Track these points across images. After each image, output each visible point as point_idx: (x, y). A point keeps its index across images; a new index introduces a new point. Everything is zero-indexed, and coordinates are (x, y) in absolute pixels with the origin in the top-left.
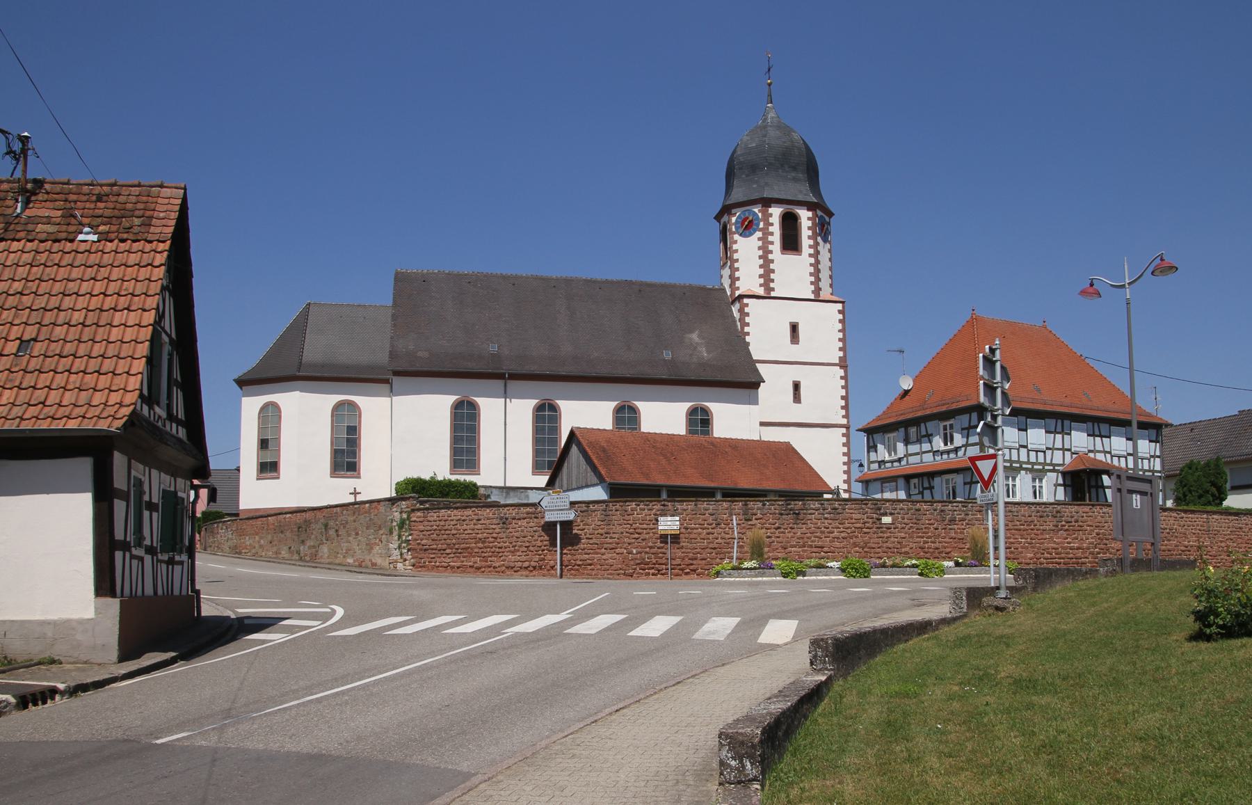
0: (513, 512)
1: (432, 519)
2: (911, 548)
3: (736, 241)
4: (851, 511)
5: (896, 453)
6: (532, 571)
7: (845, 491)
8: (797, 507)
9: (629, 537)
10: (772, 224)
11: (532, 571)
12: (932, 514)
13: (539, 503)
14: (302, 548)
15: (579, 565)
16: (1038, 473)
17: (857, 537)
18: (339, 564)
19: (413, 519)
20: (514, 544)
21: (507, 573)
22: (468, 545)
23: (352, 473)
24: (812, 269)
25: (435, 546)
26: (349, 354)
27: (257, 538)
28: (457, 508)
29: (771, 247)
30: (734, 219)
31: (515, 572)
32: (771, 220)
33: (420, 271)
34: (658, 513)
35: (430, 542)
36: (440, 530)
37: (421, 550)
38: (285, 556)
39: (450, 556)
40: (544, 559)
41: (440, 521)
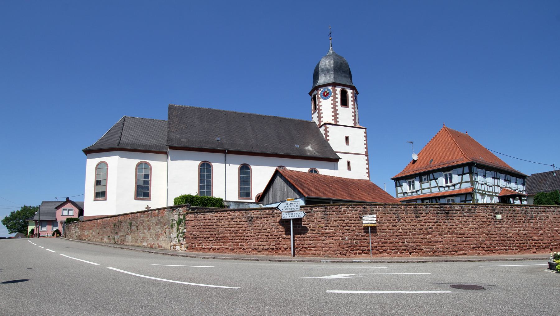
0: (257, 213)
1: (200, 219)
2: (513, 234)
3: (321, 101)
4: (479, 211)
5: (414, 188)
6: (271, 251)
7: (491, 199)
8: (447, 209)
9: (342, 229)
10: (337, 94)
11: (271, 251)
12: (521, 213)
13: (277, 207)
14: (116, 237)
15: (305, 248)
16: (491, 197)
17: (483, 227)
18: (138, 246)
19: (187, 219)
20: (257, 234)
21: (253, 253)
22: (225, 235)
23: (146, 198)
24: (353, 114)
25: (202, 236)
26: (144, 140)
27: (91, 231)
28: (217, 212)
29: (337, 104)
30: (320, 92)
31: (258, 252)
32: (336, 92)
33: (181, 106)
34: (361, 213)
35: (198, 233)
36: (205, 225)
37: (192, 238)
38: (106, 241)
39: (212, 242)
40: (279, 244)
41: (205, 220)
